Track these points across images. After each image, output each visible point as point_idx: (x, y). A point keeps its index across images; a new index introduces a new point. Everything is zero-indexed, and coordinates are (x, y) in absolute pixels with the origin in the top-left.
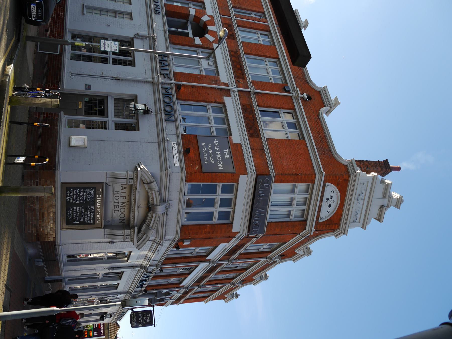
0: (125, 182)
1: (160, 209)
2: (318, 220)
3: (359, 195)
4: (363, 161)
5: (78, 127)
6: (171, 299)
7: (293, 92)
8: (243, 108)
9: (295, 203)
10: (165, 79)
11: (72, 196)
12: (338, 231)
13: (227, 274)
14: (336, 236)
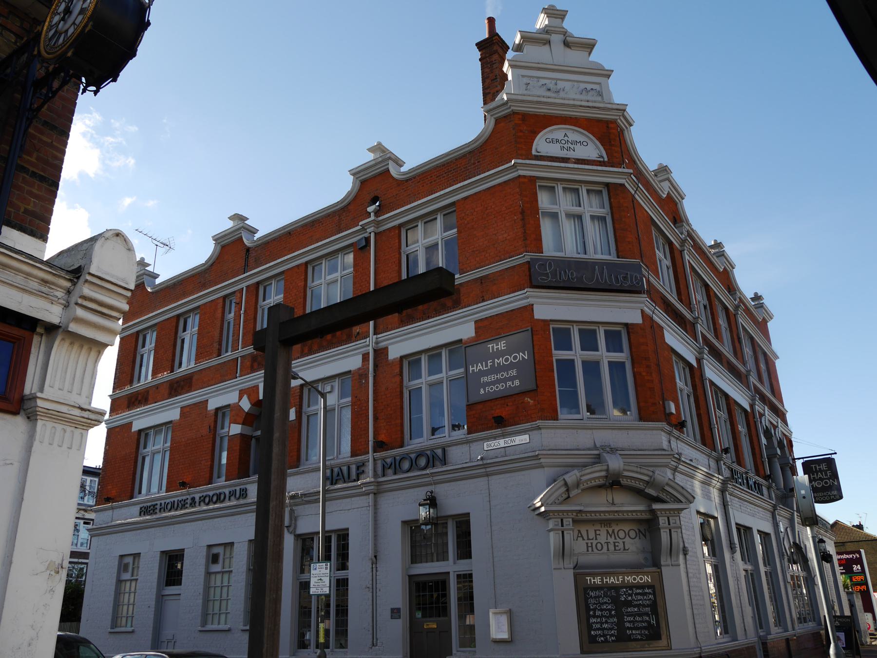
0: (570, 534)
1: (615, 463)
2: (604, 162)
3: (549, 90)
4: (484, 89)
5: (472, 628)
6: (777, 427)
7: (367, 232)
8: (408, 323)
9: (576, 210)
10: (366, 470)
11: (606, 632)
12: (621, 122)
13: (720, 322)
14: (631, 125)
